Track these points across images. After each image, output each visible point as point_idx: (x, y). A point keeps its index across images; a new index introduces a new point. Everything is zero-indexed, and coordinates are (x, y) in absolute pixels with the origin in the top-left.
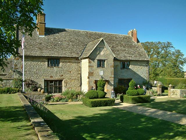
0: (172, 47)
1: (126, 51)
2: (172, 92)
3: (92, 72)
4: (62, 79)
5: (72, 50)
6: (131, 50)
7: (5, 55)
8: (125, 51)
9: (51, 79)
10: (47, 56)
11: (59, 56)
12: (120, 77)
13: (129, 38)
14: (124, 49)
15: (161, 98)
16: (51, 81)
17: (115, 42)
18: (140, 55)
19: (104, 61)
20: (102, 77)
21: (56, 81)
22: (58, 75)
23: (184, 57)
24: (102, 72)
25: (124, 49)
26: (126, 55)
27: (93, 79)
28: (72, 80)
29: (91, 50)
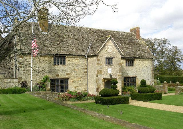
0: (169, 44)
1: (130, 48)
2: (180, 89)
3: (100, 69)
4: (68, 78)
5: (77, 47)
6: (135, 47)
7: (16, 60)
8: (129, 48)
9: (57, 78)
10: (53, 53)
11: (66, 54)
12: (125, 75)
13: (131, 35)
14: (128, 46)
15: (165, 95)
16: (58, 80)
17: (118, 39)
18: (145, 53)
19: (112, 58)
20: (110, 75)
21: (62, 80)
22: (64, 74)
23: (182, 54)
24: (111, 69)
25: (128, 46)
26: (131, 52)
27: (101, 77)
28: (78, 78)
29: (99, 48)
